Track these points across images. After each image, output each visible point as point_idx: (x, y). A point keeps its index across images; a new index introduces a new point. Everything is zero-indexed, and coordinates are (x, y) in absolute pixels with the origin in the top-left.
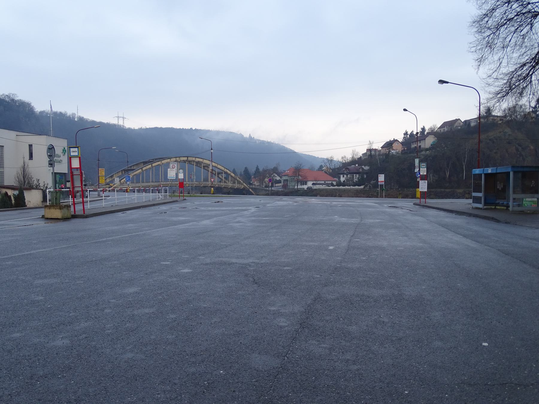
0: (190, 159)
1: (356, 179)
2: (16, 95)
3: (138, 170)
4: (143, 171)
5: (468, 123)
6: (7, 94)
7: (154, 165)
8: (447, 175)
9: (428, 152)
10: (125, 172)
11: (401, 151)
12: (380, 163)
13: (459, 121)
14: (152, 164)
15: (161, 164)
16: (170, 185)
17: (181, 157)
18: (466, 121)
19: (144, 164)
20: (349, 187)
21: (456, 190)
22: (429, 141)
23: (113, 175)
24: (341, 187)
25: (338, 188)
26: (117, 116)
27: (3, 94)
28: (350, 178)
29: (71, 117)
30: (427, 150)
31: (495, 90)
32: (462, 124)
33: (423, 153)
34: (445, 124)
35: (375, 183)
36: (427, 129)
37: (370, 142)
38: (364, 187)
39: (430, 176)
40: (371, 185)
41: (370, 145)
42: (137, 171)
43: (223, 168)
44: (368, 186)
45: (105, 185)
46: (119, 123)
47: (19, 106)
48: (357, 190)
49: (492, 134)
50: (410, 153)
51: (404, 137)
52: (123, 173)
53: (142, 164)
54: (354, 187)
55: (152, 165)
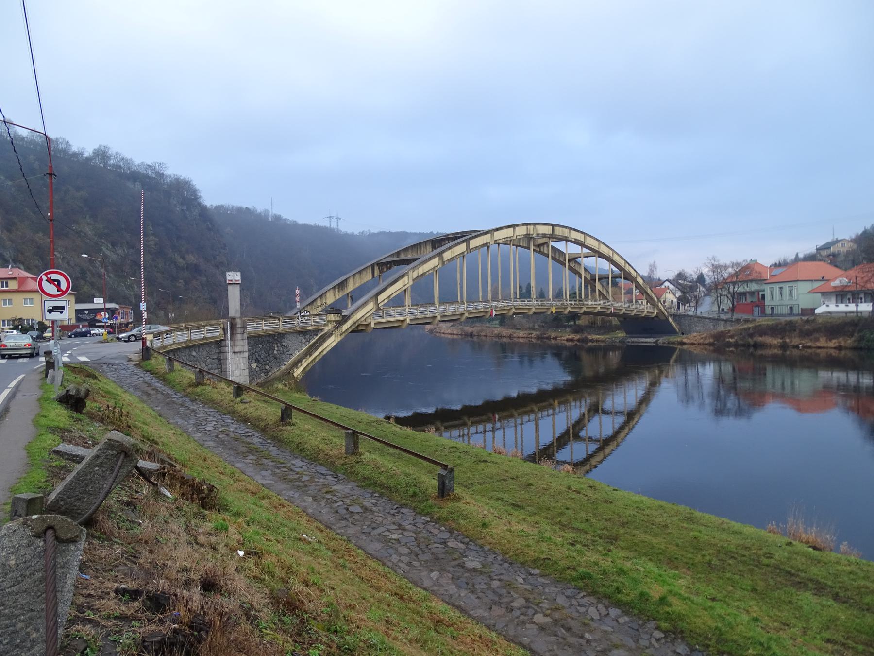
2: (165, 164)
4: (443, 263)
6: (150, 164)
10: (381, 272)
19: (435, 249)
23: (346, 280)
27: (142, 163)
29: (263, 214)
42: (429, 263)
45: (319, 315)
46: (332, 226)
47: (170, 185)
52: (377, 273)
53: (429, 248)
55: (468, 246)
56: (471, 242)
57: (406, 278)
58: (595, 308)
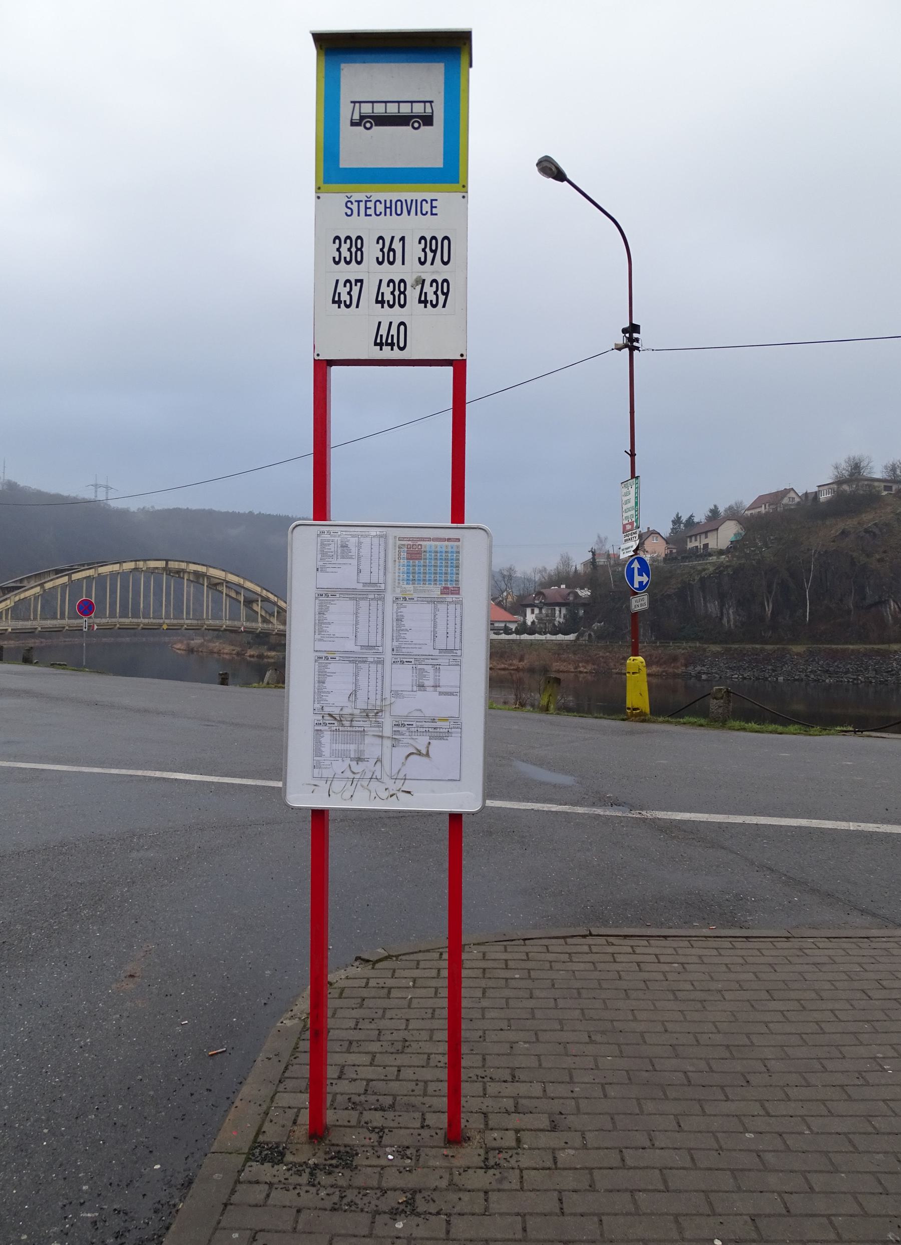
0: (173, 565)
1: (560, 617)
3: (32, 588)
5: (811, 497)
7: (75, 577)
8: (769, 611)
9: (724, 557)
11: (663, 555)
12: (614, 581)
13: (792, 495)
14: (70, 575)
15: (97, 575)
16: (118, 626)
17: (149, 560)
18: (806, 494)
20: (543, 637)
21: (790, 647)
22: (727, 534)
24: (525, 637)
25: (517, 637)
26: (93, 483)
28: (547, 616)
30: (721, 552)
31: (859, 460)
32: (797, 500)
33: (713, 559)
34: (761, 501)
35: (601, 627)
36: (721, 509)
37: (599, 537)
38: (578, 638)
39: (728, 614)
40: (592, 633)
41: (601, 545)
43: (258, 589)
44: (587, 634)
48: (560, 644)
49: (868, 518)
50: (684, 559)
51: (672, 529)
54: (554, 637)
55: (70, 578)
56: (72, 575)
57: (8, 602)
58: (222, 626)
